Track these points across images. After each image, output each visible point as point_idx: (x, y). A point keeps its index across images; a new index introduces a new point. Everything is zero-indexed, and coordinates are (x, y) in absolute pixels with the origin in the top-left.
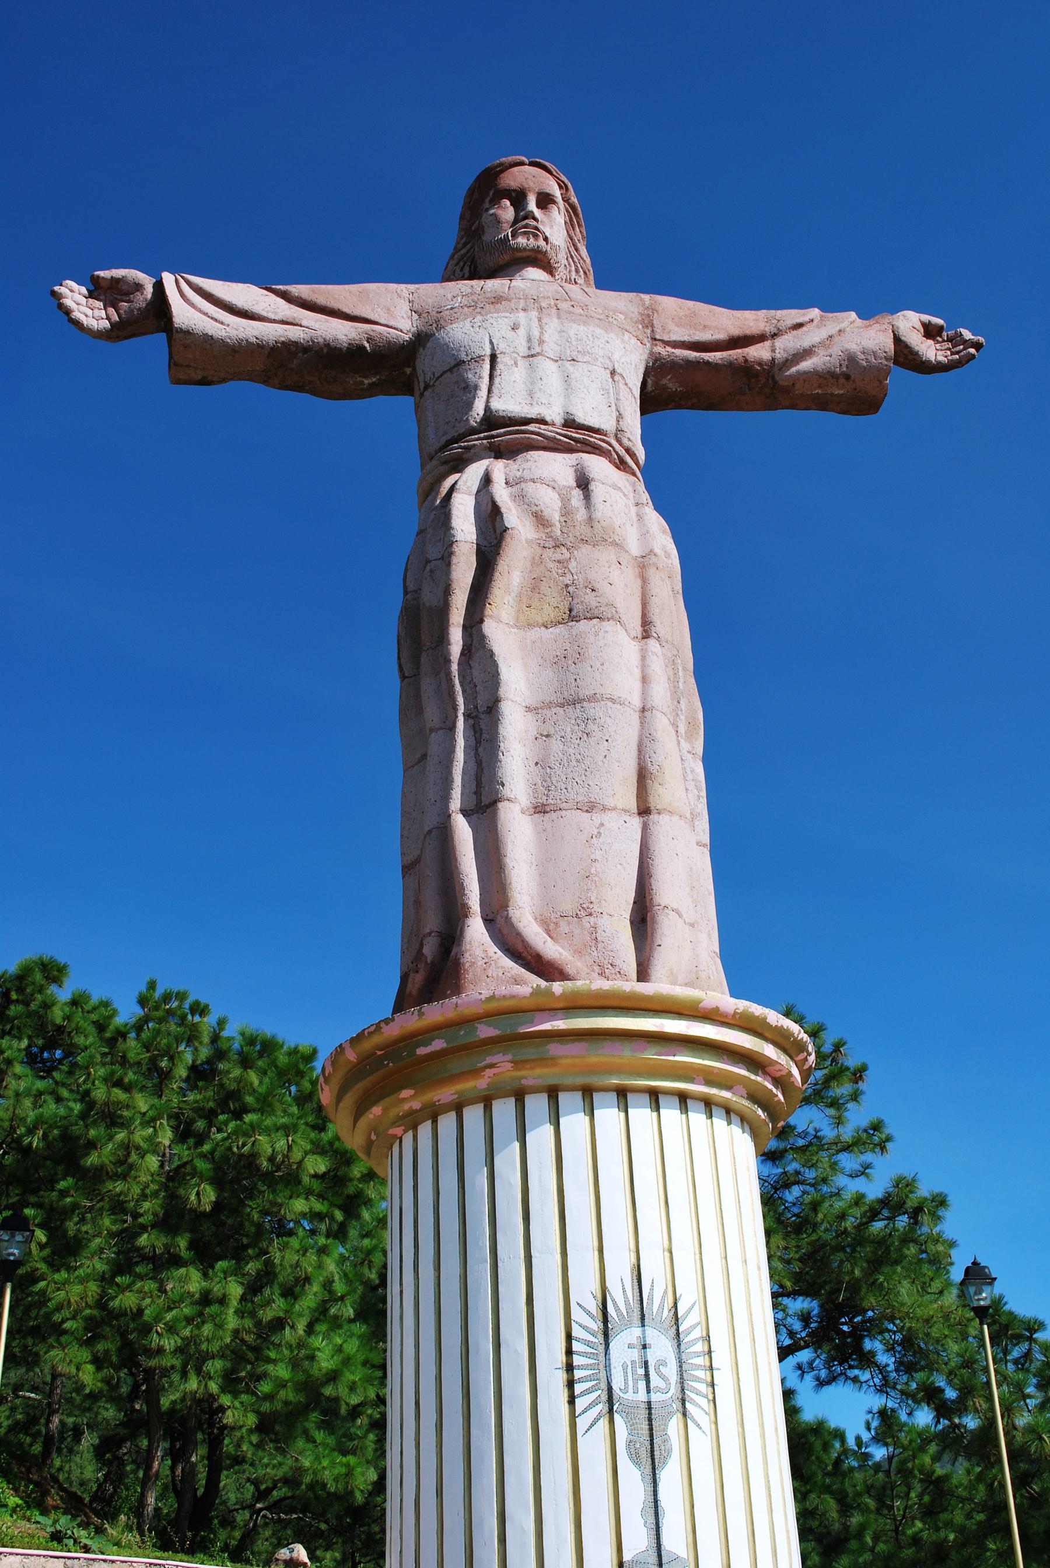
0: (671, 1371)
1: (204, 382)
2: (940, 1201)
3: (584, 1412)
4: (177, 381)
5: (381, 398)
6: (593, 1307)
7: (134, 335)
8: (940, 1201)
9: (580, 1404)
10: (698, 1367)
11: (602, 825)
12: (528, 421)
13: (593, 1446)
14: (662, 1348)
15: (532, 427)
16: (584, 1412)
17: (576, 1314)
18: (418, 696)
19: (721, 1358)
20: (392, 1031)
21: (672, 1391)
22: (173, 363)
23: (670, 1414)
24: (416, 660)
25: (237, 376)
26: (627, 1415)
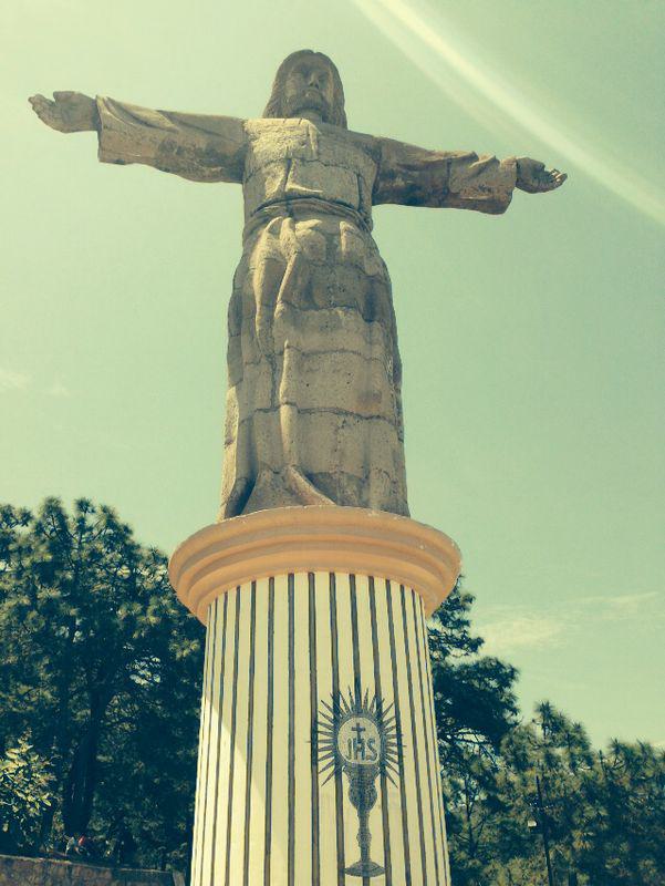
0: (377, 746)
1: (119, 162)
2: (469, 599)
3: (324, 769)
4: (103, 160)
5: (221, 184)
6: (330, 703)
7: (78, 130)
8: (469, 599)
9: (393, 723)
10: (393, 745)
11: (344, 422)
12: (308, 197)
13: (327, 790)
14: (371, 731)
15: (312, 200)
16: (324, 769)
17: (321, 708)
18: (239, 346)
19: (407, 740)
20: (221, 535)
21: (378, 759)
22: (101, 147)
23: (376, 774)
24: (239, 325)
25: (139, 161)
26: (349, 772)
